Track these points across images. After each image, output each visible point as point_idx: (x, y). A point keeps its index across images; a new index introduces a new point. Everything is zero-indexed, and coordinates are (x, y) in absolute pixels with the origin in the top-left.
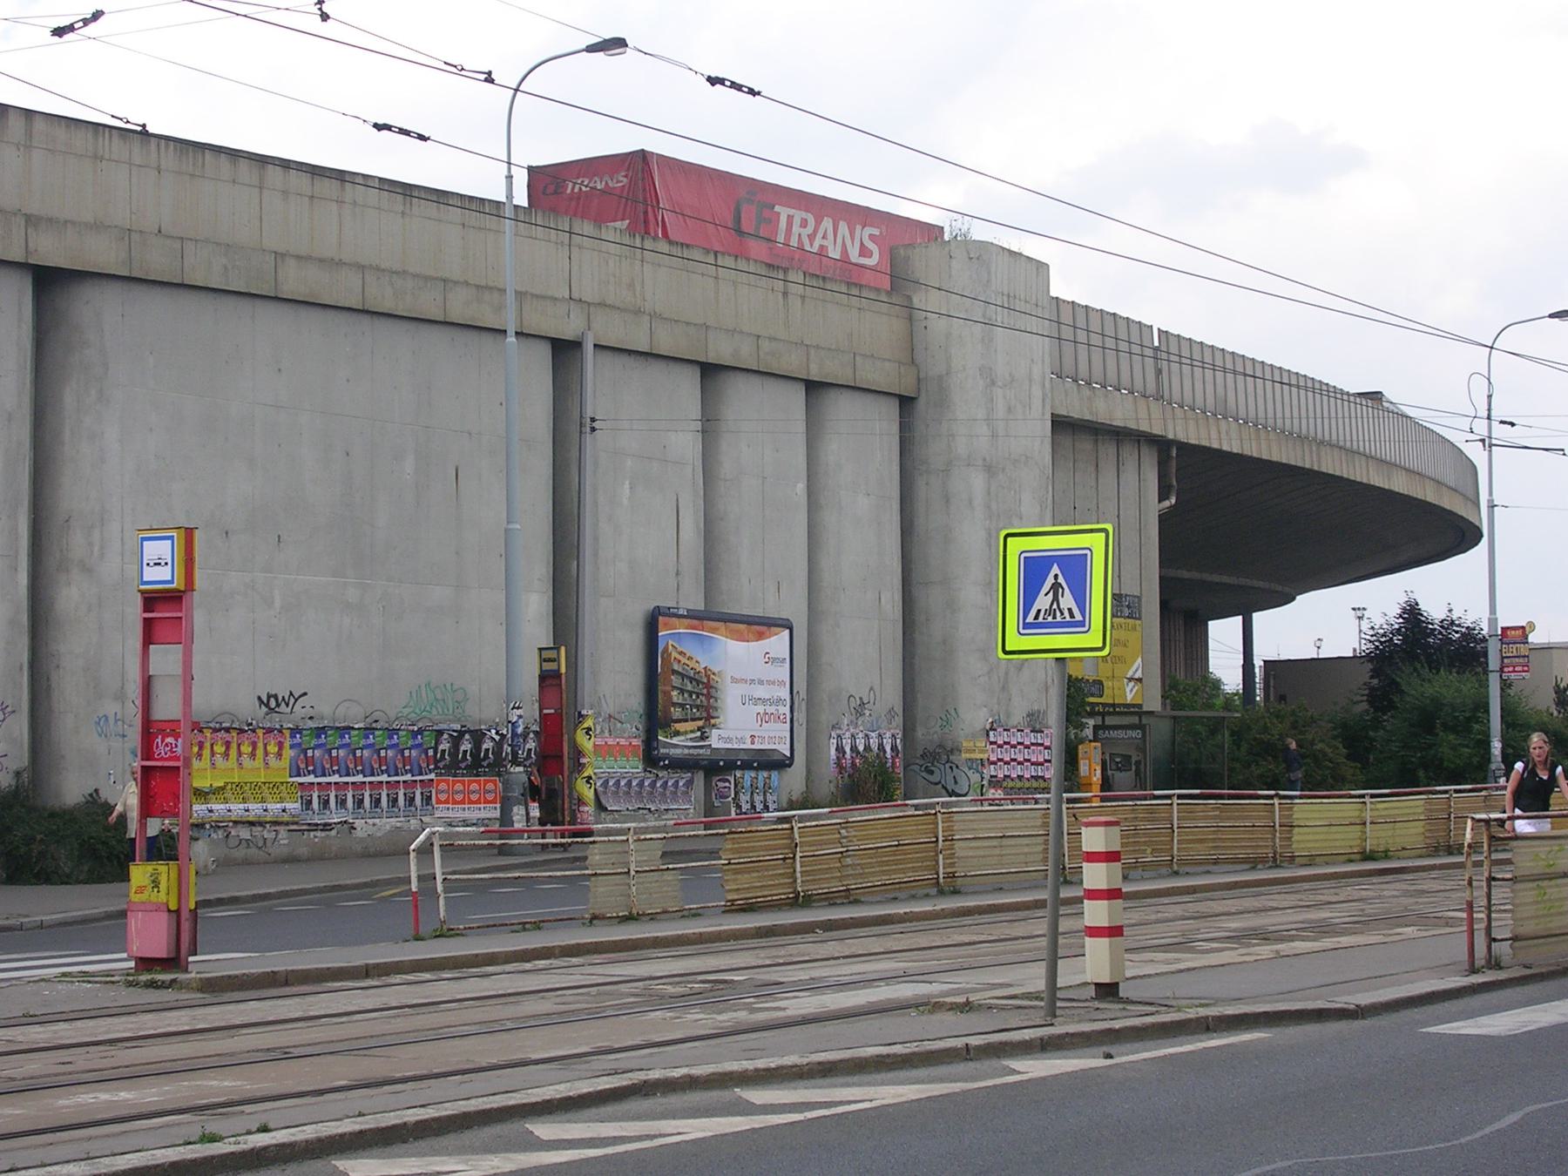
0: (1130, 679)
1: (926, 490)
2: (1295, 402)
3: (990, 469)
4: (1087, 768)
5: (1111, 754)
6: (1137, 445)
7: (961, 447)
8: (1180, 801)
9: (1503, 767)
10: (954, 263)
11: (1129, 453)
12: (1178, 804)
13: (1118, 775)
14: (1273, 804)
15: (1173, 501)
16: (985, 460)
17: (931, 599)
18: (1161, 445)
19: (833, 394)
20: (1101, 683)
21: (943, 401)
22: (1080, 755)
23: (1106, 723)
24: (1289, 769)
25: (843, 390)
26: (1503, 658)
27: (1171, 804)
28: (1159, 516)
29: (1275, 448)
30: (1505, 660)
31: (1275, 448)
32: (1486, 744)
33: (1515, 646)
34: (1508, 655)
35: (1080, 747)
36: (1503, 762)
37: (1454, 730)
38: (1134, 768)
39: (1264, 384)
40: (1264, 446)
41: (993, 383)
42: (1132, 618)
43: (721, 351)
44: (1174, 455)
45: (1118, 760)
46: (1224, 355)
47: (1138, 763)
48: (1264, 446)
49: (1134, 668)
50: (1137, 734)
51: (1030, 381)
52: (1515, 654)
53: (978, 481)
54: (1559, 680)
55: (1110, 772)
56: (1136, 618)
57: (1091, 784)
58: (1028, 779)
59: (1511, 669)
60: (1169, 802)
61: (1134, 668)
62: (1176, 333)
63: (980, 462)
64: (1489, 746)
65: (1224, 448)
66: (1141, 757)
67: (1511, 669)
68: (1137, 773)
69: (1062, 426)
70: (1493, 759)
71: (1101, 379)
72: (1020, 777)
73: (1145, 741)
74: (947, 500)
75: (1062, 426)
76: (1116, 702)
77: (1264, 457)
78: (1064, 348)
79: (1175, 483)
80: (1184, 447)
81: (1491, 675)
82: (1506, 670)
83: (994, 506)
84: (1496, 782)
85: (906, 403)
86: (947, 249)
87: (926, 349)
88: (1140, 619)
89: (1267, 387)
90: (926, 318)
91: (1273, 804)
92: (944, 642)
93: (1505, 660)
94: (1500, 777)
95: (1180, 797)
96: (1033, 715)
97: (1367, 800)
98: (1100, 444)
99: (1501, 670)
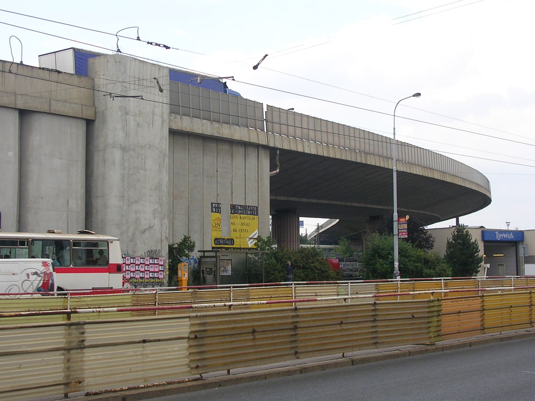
0: (251, 238)
1: (97, 158)
2: (454, 163)
3: (124, 149)
4: (181, 274)
5: (206, 268)
6: (257, 149)
7: (110, 140)
8: (351, 284)
9: (399, 272)
10: (109, 64)
11: (252, 153)
12: (350, 285)
13: (208, 276)
14: (441, 282)
15: (278, 171)
16: (121, 145)
17: (98, 203)
18: (272, 151)
19: (37, 117)
20: (233, 240)
21: (104, 122)
22: (179, 269)
23: (205, 255)
24: (288, 274)
25: (45, 115)
26: (398, 230)
27: (398, 283)
28: (270, 177)
29: (429, 173)
30: (400, 231)
31: (429, 173)
32: (392, 263)
33: (402, 225)
34: (400, 228)
35: (179, 265)
36: (399, 270)
37: (383, 258)
38: (213, 273)
39: (408, 148)
40: (363, 158)
41: (127, 113)
42: (252, 215)
43: (30, 105)
44: (278, 153)
45: (208, 270)
46: (373, 135)
47: (214, 271)
48: (363, 158)
49: (253, 234)
50: (214, 259)
51: (153, 114)
52: (402, 228)
53: (117, 154)
54: (449, 239)
55: (205, 275)
56: (255, 215)
57: (182, 280)
58: (148, 279)
59: (401, 234)
60: (397, 283)
61: (253, 234)
62: (381, 135)
63: (118, 146)
64: (394, 264)
65: (306, 152)
66: (215, 269)
67: (401, 234)
68: (214, 275)
69: (174, 133)
70: (395, 269)
71: (278, 132)
72: (142, 278)
73: (217, 262)
74: (104, 162)
75: (174, 133)
76: (241, 247)
77: (382, 166)
78: (329, 136)
79: (279, 164)
80: (284, 152)
81: (395, 236)
82: (400, 234)
83: (126, 164)
84: (396, 278)
85: (89, 123)
86: (107, 59)
87: (99, 100)
88: (257, 215)
89: (409, 149)
90: (99, 87)
91: (441, 282)
92: (102, 221)
93: (400, 231)
94: (397, 276)
95: (351, 283)
96: (151, 252)
97: (69, 296)
98: (175, 137)
99: (398, 235)
